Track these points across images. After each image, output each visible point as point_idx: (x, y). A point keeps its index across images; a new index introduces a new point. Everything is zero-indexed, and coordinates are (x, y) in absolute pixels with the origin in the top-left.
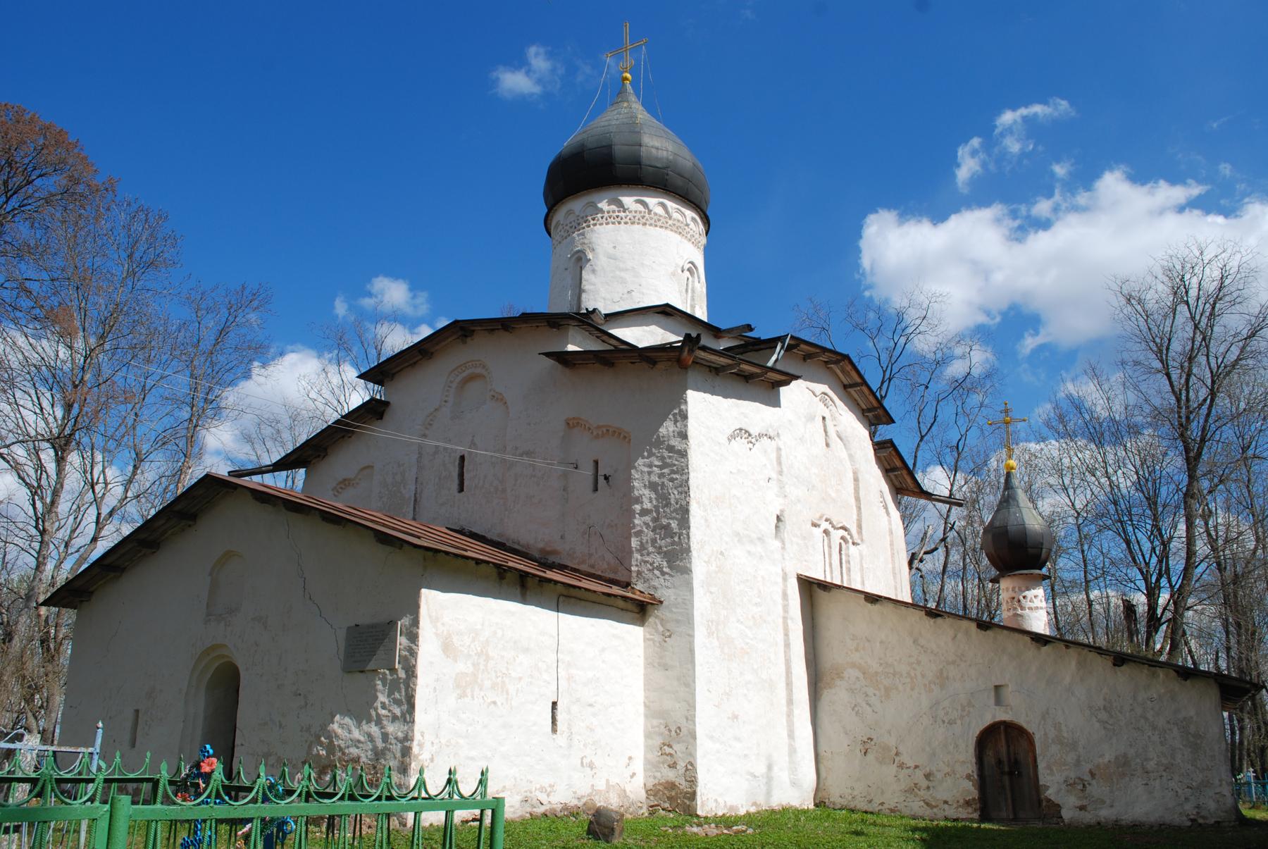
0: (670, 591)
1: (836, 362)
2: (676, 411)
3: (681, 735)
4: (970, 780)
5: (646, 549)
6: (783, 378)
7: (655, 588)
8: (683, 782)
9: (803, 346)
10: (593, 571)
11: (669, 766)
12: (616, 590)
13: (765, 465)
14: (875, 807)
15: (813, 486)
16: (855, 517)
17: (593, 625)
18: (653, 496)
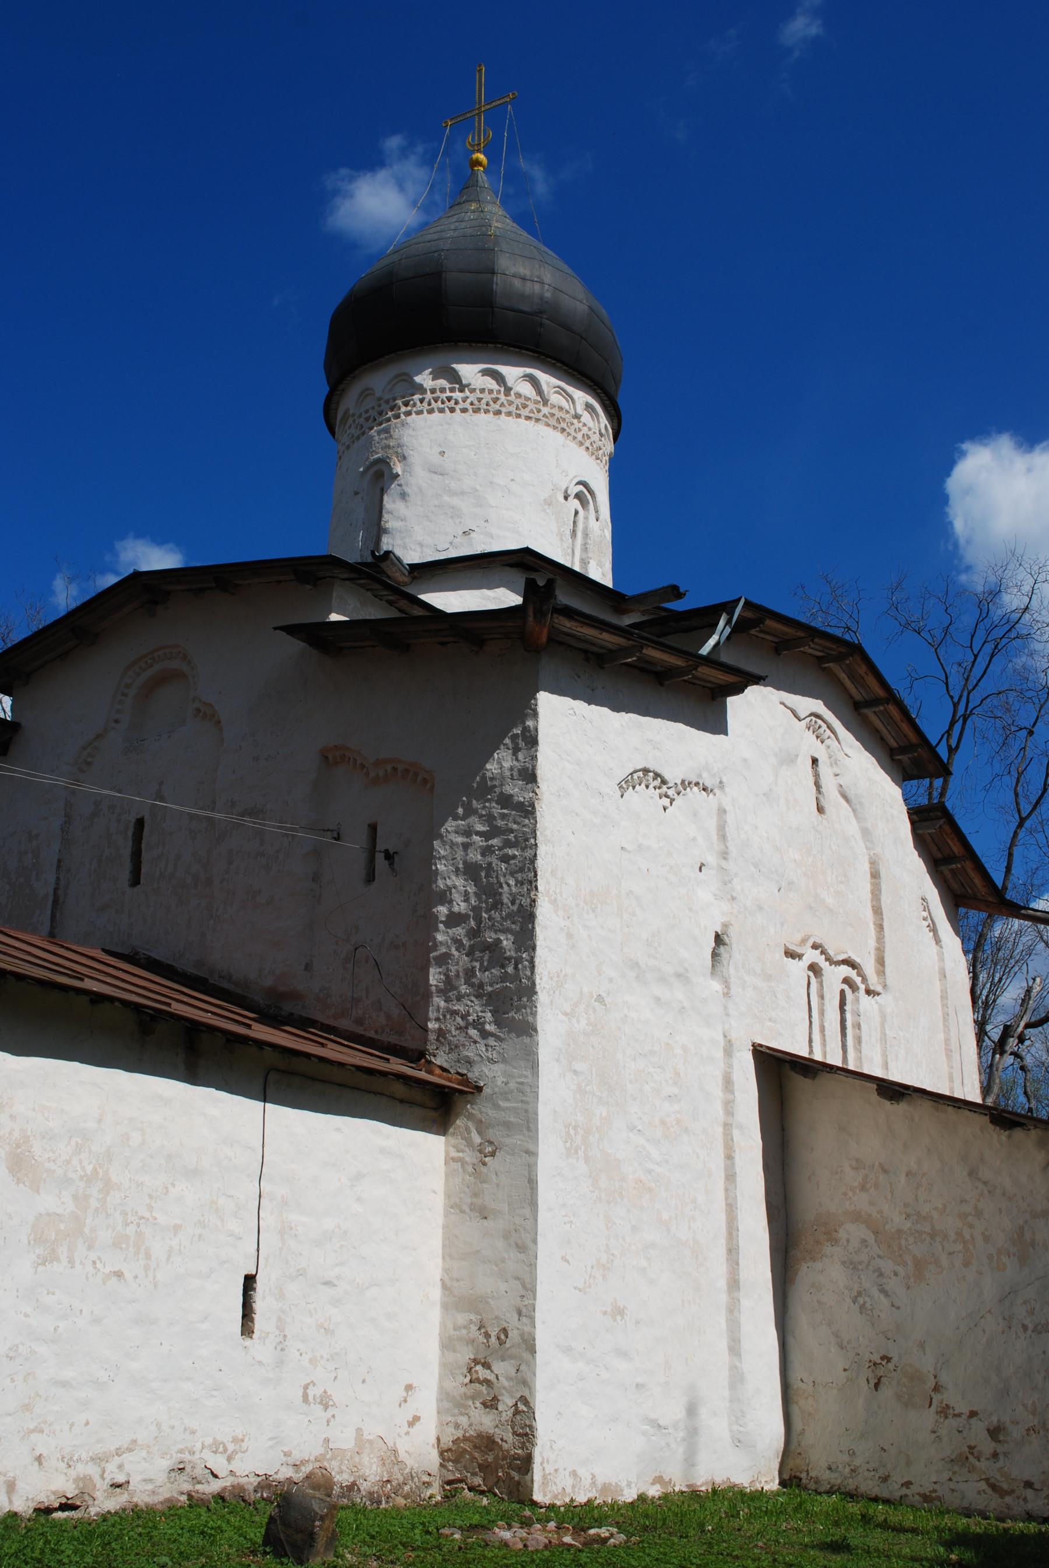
0: (495, 1067)
1: (839, 659)
2: (517, 731)
3: (507, 1345)
5: (455, 988)
6: (731, 679)
7: (470, 1062)
8: (509, 1437)
9: (770, 623)
10: (360, 1030)
11: (484, 1404)
12: (397, 1065)
13: (694, 839)
14: (894, 1489)
15: (791, 883)
16: (872, 943)
17: (338, 1130)
18: (471, 889)
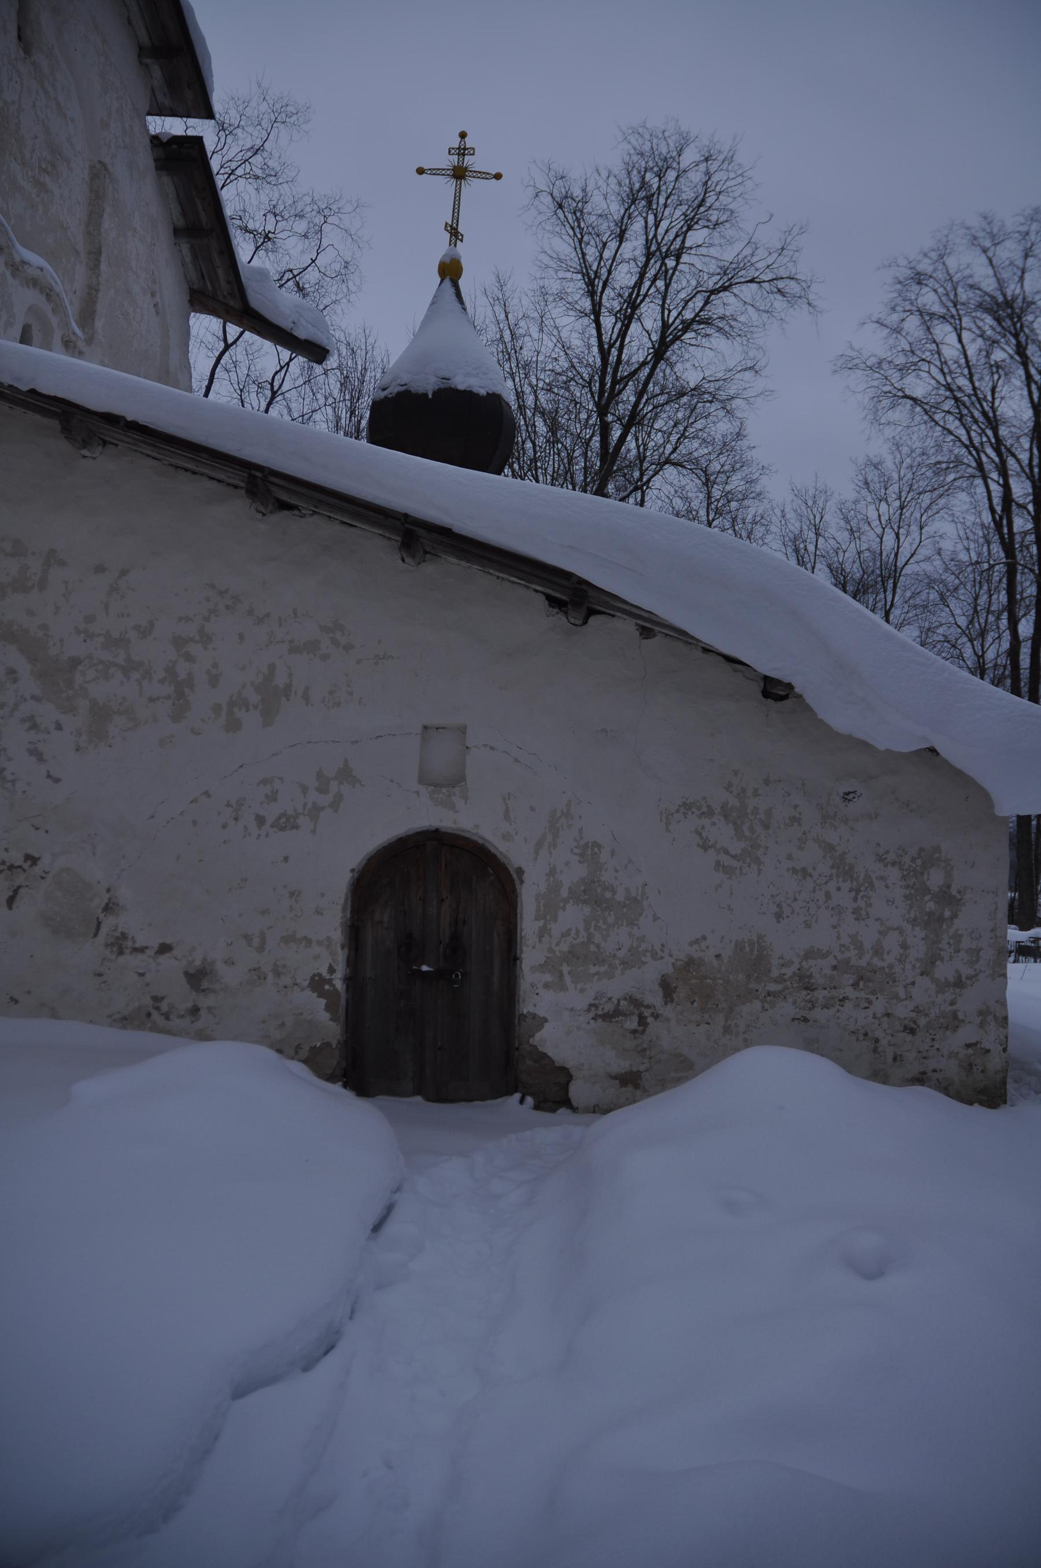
4: (321, 994)
